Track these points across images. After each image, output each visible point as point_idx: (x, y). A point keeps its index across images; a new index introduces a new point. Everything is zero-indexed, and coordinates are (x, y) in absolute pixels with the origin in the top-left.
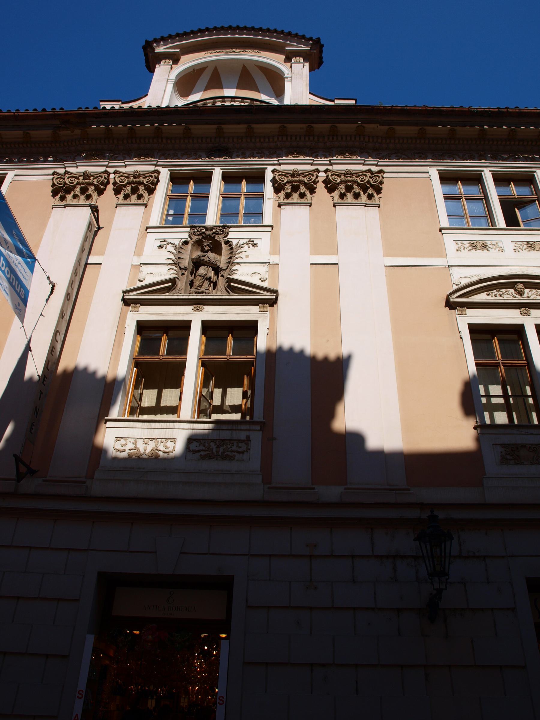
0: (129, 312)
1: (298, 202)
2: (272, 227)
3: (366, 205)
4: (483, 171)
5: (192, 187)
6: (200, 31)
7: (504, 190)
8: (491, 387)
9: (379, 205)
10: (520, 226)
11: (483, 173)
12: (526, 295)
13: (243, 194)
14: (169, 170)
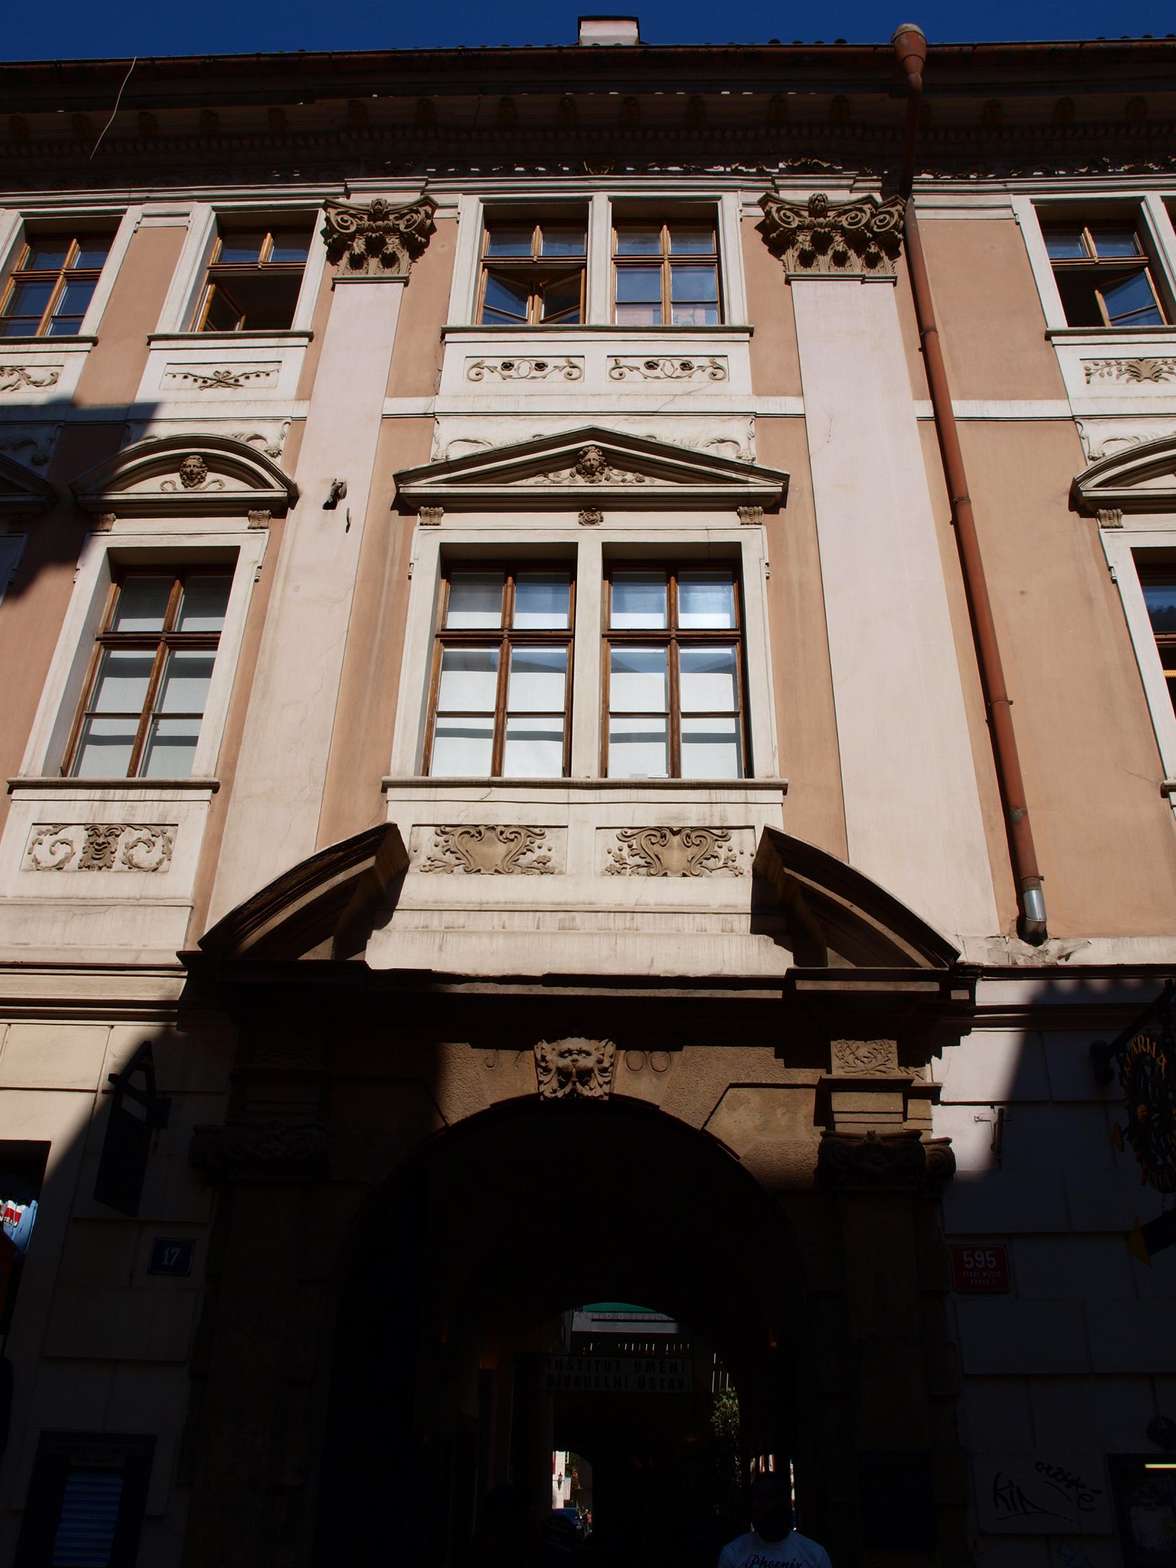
1: (798, 273)
2: (750, 331)
3: (863, 280)
4: (720, 198)
5: (666, 242)
10: (1103, 324)
11: (719, 203)
13: (666, 257)
14: (214, 209)
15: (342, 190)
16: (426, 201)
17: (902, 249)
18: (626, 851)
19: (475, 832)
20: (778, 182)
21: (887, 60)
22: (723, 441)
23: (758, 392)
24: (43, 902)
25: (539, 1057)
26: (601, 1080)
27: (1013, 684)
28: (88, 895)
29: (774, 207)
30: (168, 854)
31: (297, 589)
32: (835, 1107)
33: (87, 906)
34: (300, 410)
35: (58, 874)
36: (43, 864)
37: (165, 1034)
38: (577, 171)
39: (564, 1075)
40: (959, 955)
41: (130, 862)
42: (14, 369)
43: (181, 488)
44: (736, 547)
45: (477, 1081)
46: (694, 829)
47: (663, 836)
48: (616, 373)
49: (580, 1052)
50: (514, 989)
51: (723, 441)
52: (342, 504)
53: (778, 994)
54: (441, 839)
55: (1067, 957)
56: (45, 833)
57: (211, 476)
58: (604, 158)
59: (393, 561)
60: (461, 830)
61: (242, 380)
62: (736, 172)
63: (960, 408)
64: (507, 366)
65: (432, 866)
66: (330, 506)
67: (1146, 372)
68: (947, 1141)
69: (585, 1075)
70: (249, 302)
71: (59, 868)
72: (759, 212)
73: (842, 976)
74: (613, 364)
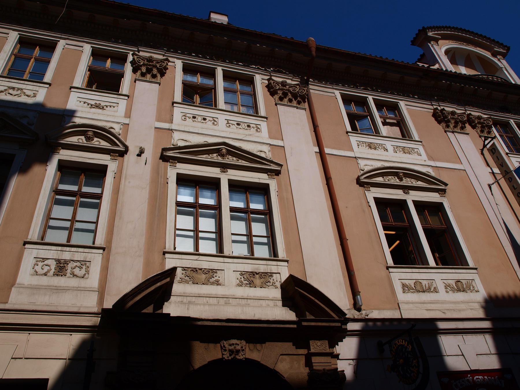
0: (169, 167)
2: (128, 96)
3: (297, 108)
6: (446, 27)
7: (190, 78)
8: (254, 225)
9: (160, 84)
12: (404, 181)
14: (92, 47)
15: (136, 50)
16: (167, 60)
17: (306, 100)
18: (242, 279)
19: (195, 270)
20: (272, 74)
21: (305, 47)
22: (261, 151)
23: (271, 137)
24: (40, 287)
25: (222, 345)
26: (242, 353)
27: (348, 234)
28: (58, 285)
29: (272, 82)
30: (88, 272)
31: (129, 182)
32: (313, 361)
33: (58, 290)
34: (127, 121)
35: (45, 278)
36: (39, 273)
37: (92, 337)
38: (211, 59)
39: (231, 352)
40: (346, 315)
41: (73, 274)
42: (18, 89)
43: (85, 142)
44: (219, 179)
45: (204, 354)
46: (263, 273)
47: (254, 275)
48: (228, 125)
49: (236, 344)
50: (216, 324)
51: (261, 151)
52: (143, 155)
53: (295, 326)
54: (184, 272)
55: (367, 316)
56: (39, 261)
57: (96, 139)
58: (221, 57)
59: (161, 177)
60: (190, 269)
61: (105, 107)
62: (258, 68)
63: (327, 151)
64: (194, 117)
65: (182, 281)
66: (139, 155)
67: (372, 147)
68: (344, 371)
69: (238, 352)
70: (103, 81)
71: (45, 274)
72: (267, 82)
73: (311, 321)
74: (227, 122)
